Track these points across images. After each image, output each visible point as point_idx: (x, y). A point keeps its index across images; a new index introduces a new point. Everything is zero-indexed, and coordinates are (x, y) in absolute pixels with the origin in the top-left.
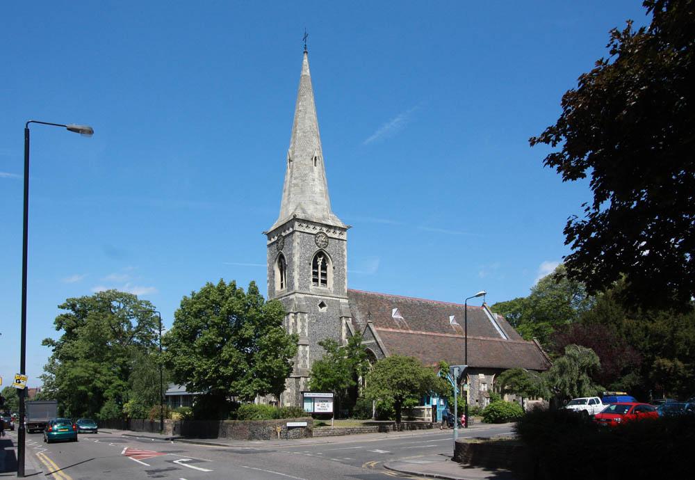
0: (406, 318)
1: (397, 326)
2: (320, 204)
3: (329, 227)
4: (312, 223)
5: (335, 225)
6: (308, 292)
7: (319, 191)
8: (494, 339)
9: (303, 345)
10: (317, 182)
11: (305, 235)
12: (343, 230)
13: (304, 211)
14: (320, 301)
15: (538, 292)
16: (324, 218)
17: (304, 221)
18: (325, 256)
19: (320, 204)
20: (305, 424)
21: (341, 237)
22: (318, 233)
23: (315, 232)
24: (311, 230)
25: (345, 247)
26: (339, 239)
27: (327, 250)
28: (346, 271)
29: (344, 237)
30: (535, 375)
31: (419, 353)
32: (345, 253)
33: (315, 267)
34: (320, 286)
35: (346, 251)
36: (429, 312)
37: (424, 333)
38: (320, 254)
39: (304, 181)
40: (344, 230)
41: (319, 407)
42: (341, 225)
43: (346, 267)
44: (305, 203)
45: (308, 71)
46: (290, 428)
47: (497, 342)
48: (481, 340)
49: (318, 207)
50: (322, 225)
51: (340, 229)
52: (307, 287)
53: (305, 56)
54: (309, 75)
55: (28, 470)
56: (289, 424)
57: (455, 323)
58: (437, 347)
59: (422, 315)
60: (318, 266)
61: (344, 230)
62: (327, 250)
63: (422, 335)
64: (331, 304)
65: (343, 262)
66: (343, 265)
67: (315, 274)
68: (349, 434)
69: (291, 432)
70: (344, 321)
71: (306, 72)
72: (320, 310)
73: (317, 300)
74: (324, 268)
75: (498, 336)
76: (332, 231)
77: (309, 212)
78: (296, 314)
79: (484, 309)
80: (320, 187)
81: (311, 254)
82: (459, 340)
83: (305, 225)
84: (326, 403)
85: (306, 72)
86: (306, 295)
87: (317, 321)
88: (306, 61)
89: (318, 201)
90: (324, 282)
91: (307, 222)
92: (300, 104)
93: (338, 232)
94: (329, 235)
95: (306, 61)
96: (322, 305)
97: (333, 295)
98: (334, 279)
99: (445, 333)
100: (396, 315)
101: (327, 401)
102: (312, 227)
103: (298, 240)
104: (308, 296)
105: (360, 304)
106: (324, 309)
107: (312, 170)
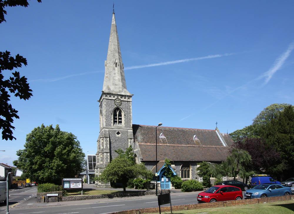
0: (167, 138)
1: (161, 142)
2: (118, 85)
3: (122, 96)
4: (112, 94)
5: (125, 94)
6: (111, 127)
7: (117, 79)
8: (147, 144)
9: (106, 153)
10: (117, 75)
11: (109, 100)
12: (129, 97)
13: (109, 89)
14: (117, 131)
15: (256, 121)
16: (120, 92)
17: (108, 94)
18: (120, 110)
19: (118, 85)
20: (57, 195)
21: (129, 100)
22: (115, 99)
23: (114, 99)
24: (112, 98)
25: (131, 105)
26: (127, 101)
27: (121, 107)
28: (132, 116)
29: (131, 100)
30: (214, 165)
31: (162, 155)
32: (131, 108)
33: (115, 115)
34: (117, 125)
35: (131, 107)
36: (182, 134)
37: (168, 145)
38: (117, 109)
39: (110, 75)
40: (131, 96)
41: (74, 185)
42: (128, 94)
43: (131, 114)
44: (110, 85)
45: (114, 22)
46: (49, 197)
47: (213, 148)
48: (204, 147)
49: (116, 86)
50: (118, 95)
51: (128, 96)
52: (110, 125)
53: (113, 15)
54: (115, 24)
55: (172, 196)
56: (48, 195)
57: (197, 139)
58: (174, 151)
59: (177, 135)
60: (117, 114)
61: (131, 96)
62: (121, 107)
63: (167, 146)
64: (123, 133)
65: (130, 112)
66: (130, 113)
67: (115, 118)
68: (86, 199)
69: (50, 199)
70: (129, 140)
71: (114, 22)
72: (117, 135)
73: (115, 131)
74: (120, 115)
75: (222, 144)
76: (124, 98)
77: (112, 89)
78: (103, 138)
79: (216, 131)
80: (118, 77)
81: (112, 109)
82: (189, 147)
83: (108, 96)
84: (78, 184)
85: (114, 22)
86: (110, 129)
87: (115, 141)
88: (113, 17)
89: (117, 84)
90: (120, 122)
91: (110, 94)
92: (110, 38)
93: (127, 98)
94: (122, 99)
95: (113, 17)
96: (118, 133)
97: (124, 128)
98: (125, 120)
99: (212, 145)
100: (195, 138)
101: (79, 182)
102: (112, 96)
103: (105, 103)
104: (111, 129)
105: (143, 132)
106: (120, 135)
107: (114, 69)
